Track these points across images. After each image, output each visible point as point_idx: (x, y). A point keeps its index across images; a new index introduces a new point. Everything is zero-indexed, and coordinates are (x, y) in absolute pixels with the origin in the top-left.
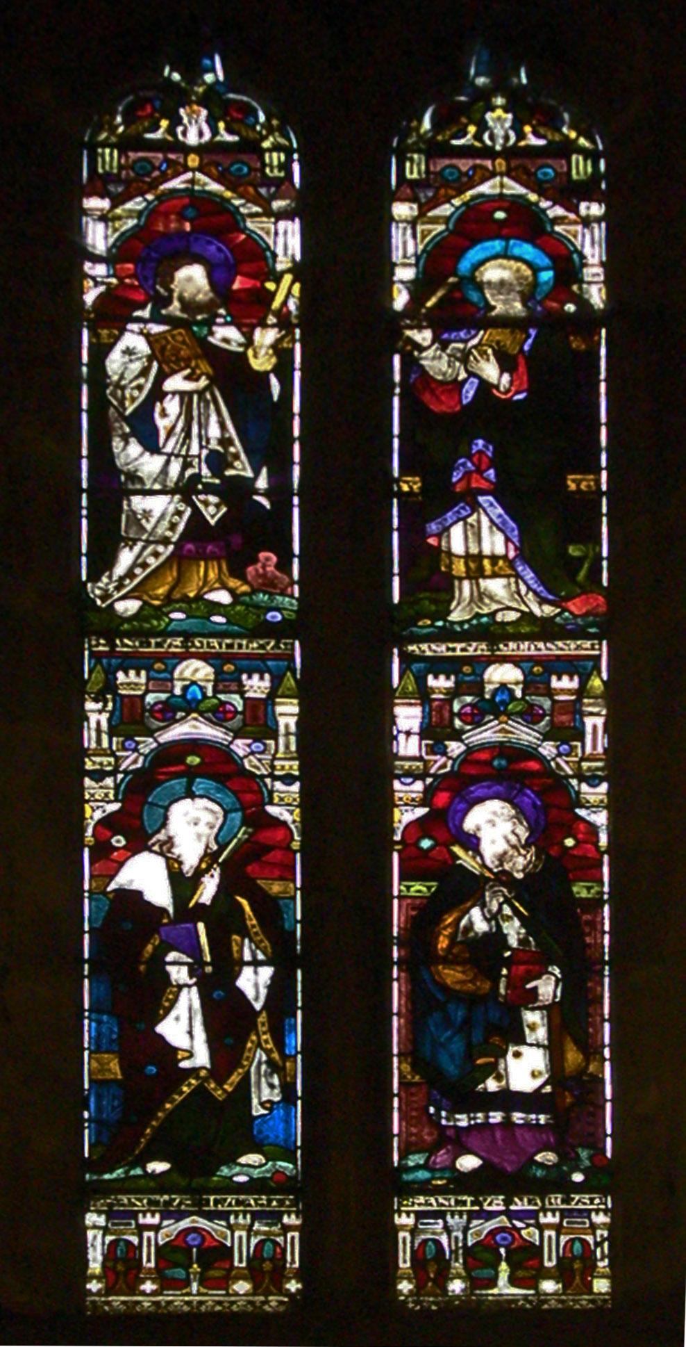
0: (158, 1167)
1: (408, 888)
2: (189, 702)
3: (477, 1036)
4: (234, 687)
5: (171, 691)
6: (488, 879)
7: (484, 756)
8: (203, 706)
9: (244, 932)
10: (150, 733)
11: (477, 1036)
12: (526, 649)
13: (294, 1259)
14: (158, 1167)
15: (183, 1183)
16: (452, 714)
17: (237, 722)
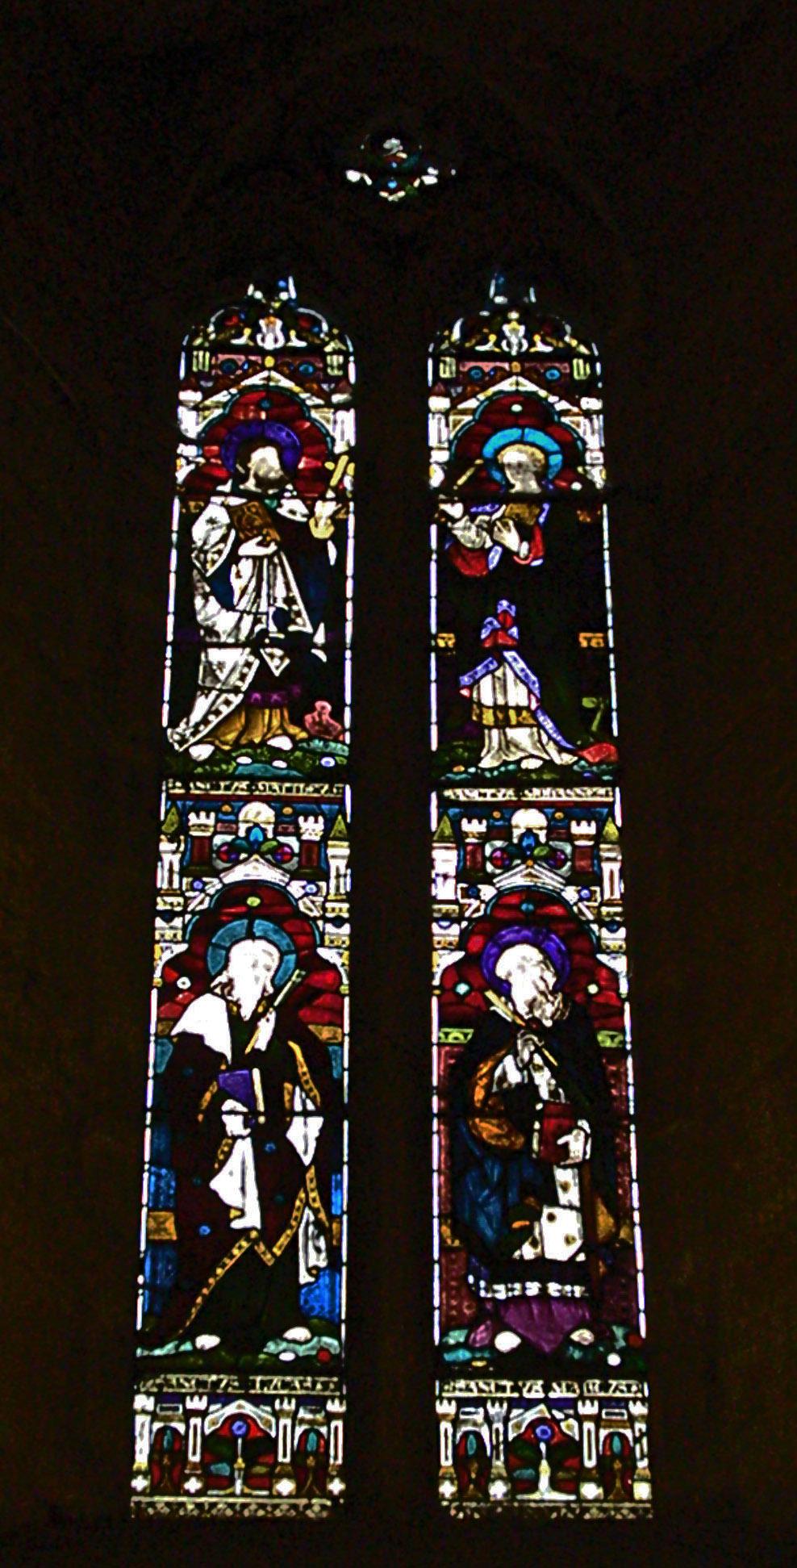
0: (208, 1341)
4: (291, 829)
6: (520, 1027)
7: (514, 900)
8: (264, 848)
9: (296, 1081)
12: (547, 794)
14: (208, 1341)
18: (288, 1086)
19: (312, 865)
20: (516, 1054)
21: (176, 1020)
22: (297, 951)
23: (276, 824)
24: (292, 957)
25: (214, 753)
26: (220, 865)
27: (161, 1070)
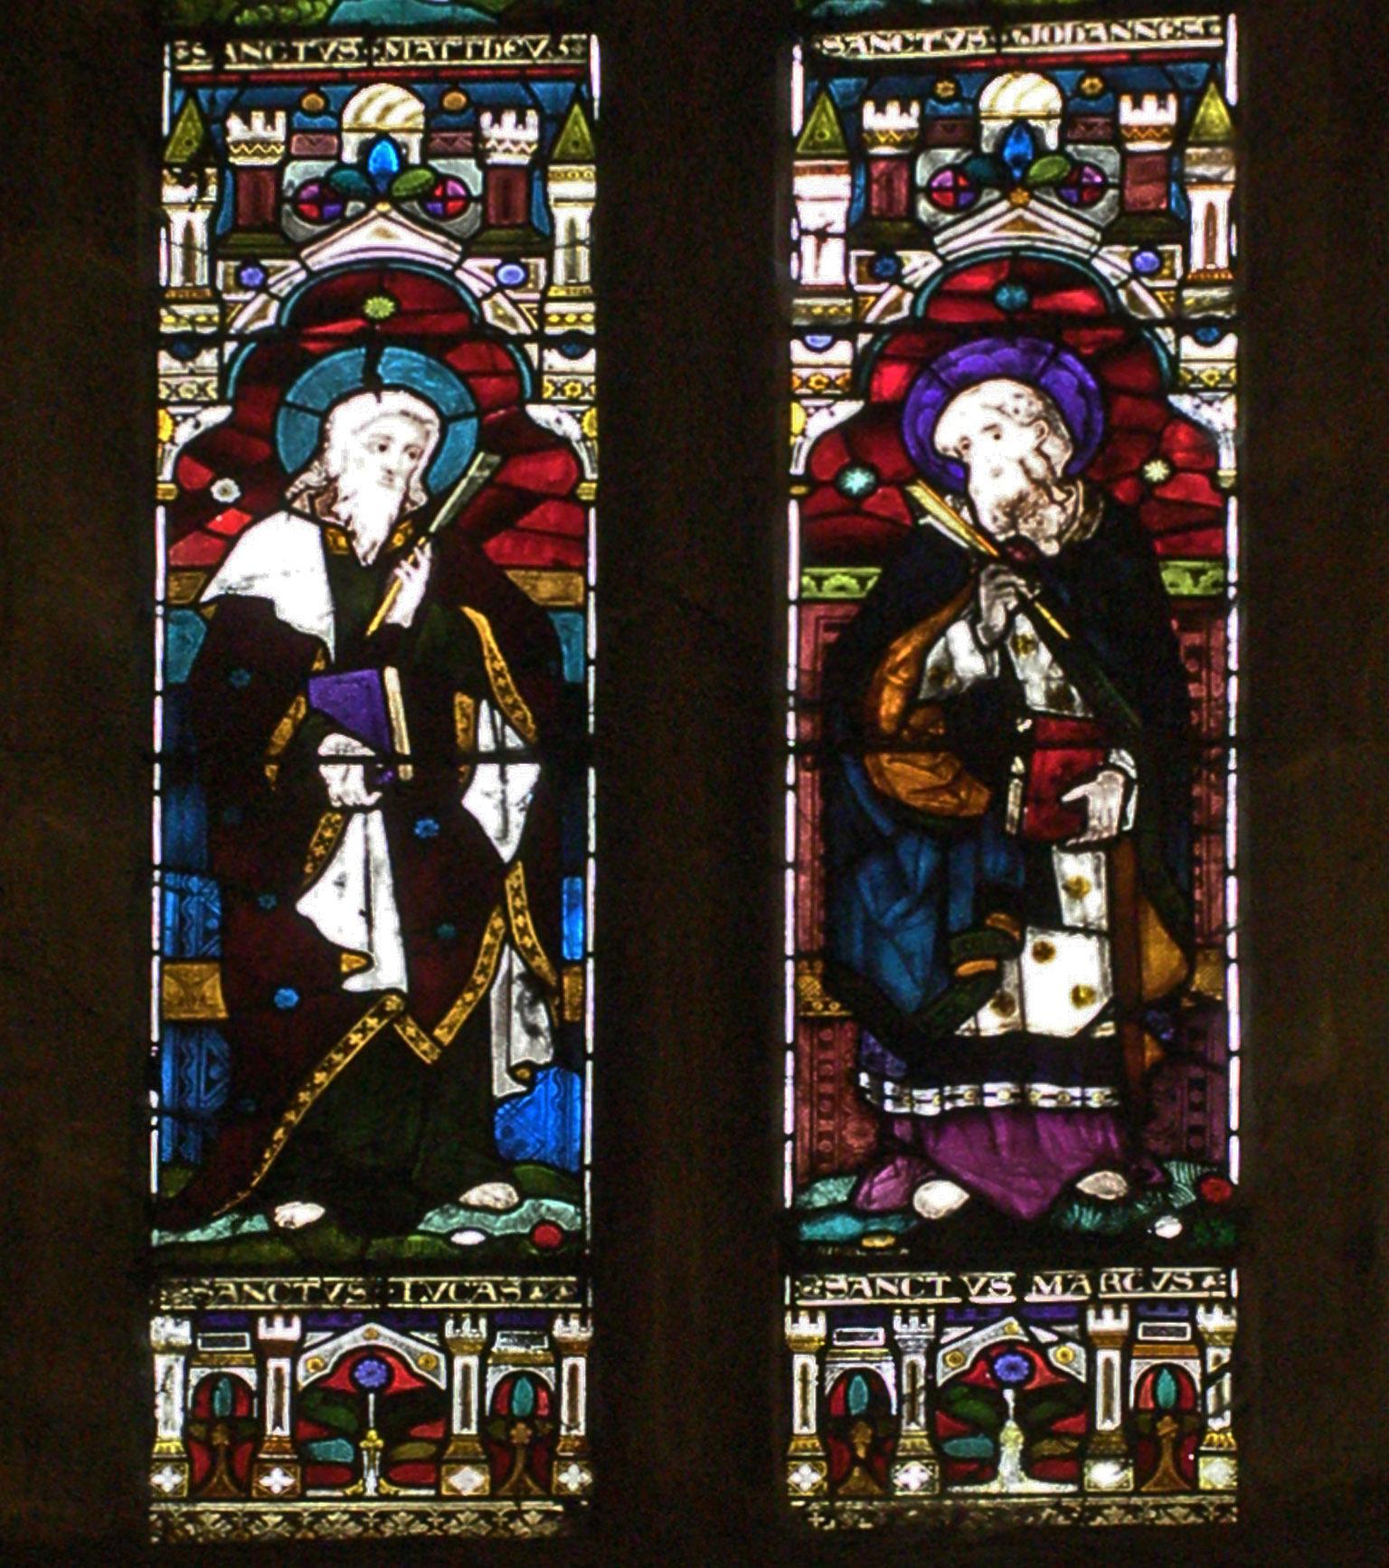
0: (300, 1213)
1: (819, 580)
3: (960, 912)
6: (985, 559)
8: (401, 188)
9: (481, 689)
11: (960, 912)
13: (575, 1421)
14: (300, 1213)
16: (914, 190)
18: (462, 699)
20: (975, 618)
21: (211, 571)
23: (428, 132)
26: (303, 228)
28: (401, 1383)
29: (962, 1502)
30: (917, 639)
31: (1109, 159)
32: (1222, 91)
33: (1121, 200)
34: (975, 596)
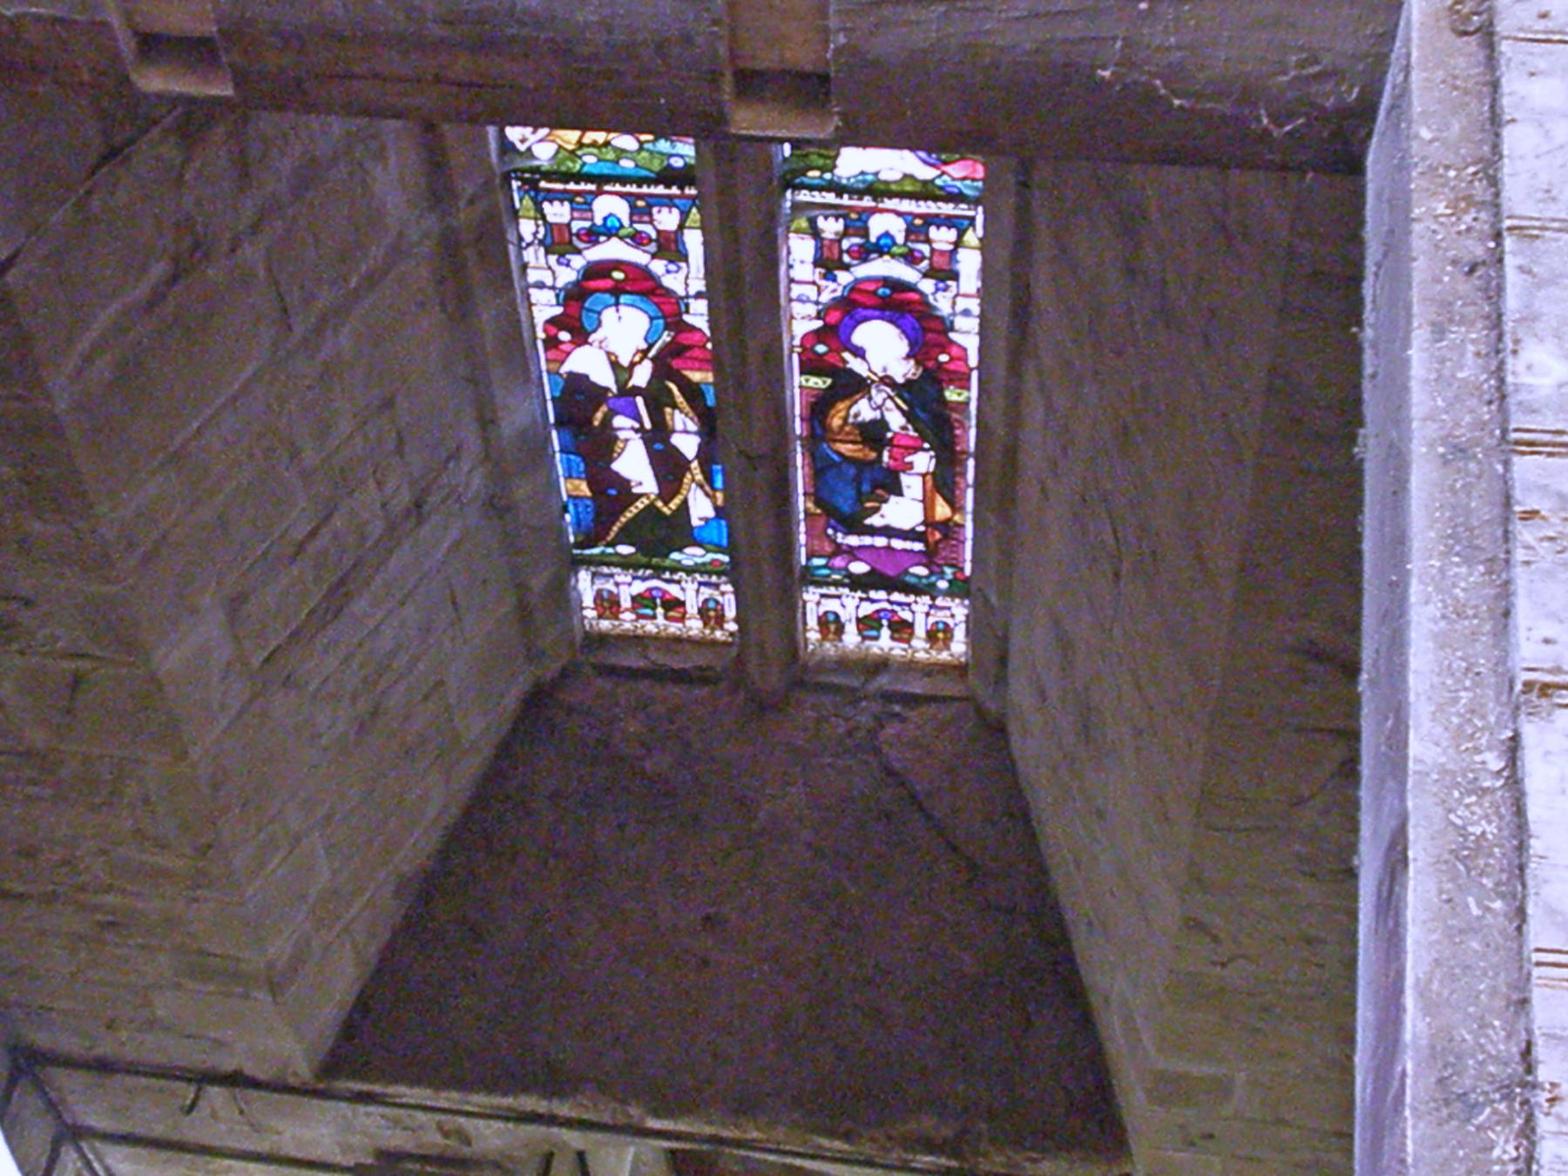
0: (625, 550)
1: (807, 381)
2: (609, 229)
3: (866, 488)
4: (646, 218)
5: (592, 219)
6: (873, 381)
7: (871, 287)
8: (623, 232)
9: (675, 406)
10: (579, 252)
11: (866, 488)
12: (907, 206)
13: (731, 612)
14: (625, 550)
15: (644, 560)
16: (841, 252)
17: (925, 264)
18: (668, 410)
19: (670, 247)
20: (870, 399)
21: (562, 362)
22: (664, 317)
23: (631, 215)
24: (661, 322)
25: (557, 152)
26: (581, 245)
27: (557, 394)
28: (667, 597)
29: (925, 173)
30: (847, 403)
31: (925, 249)
32: (974, 230)
33: (931, 264)
34: (869, 392)
